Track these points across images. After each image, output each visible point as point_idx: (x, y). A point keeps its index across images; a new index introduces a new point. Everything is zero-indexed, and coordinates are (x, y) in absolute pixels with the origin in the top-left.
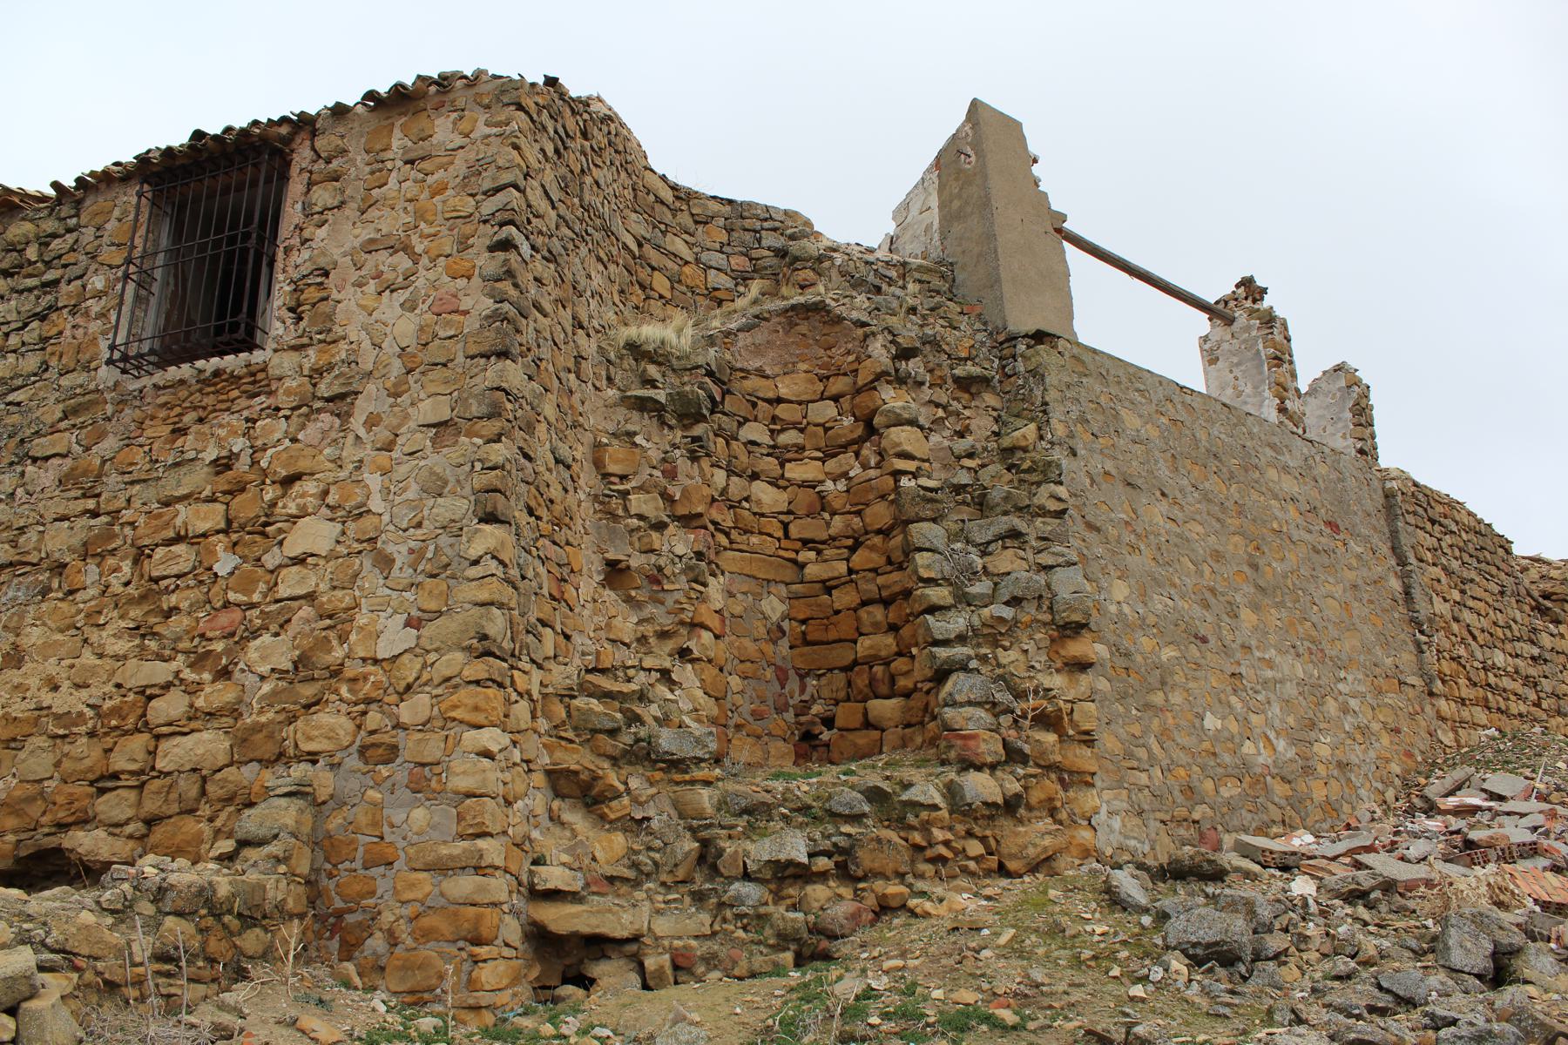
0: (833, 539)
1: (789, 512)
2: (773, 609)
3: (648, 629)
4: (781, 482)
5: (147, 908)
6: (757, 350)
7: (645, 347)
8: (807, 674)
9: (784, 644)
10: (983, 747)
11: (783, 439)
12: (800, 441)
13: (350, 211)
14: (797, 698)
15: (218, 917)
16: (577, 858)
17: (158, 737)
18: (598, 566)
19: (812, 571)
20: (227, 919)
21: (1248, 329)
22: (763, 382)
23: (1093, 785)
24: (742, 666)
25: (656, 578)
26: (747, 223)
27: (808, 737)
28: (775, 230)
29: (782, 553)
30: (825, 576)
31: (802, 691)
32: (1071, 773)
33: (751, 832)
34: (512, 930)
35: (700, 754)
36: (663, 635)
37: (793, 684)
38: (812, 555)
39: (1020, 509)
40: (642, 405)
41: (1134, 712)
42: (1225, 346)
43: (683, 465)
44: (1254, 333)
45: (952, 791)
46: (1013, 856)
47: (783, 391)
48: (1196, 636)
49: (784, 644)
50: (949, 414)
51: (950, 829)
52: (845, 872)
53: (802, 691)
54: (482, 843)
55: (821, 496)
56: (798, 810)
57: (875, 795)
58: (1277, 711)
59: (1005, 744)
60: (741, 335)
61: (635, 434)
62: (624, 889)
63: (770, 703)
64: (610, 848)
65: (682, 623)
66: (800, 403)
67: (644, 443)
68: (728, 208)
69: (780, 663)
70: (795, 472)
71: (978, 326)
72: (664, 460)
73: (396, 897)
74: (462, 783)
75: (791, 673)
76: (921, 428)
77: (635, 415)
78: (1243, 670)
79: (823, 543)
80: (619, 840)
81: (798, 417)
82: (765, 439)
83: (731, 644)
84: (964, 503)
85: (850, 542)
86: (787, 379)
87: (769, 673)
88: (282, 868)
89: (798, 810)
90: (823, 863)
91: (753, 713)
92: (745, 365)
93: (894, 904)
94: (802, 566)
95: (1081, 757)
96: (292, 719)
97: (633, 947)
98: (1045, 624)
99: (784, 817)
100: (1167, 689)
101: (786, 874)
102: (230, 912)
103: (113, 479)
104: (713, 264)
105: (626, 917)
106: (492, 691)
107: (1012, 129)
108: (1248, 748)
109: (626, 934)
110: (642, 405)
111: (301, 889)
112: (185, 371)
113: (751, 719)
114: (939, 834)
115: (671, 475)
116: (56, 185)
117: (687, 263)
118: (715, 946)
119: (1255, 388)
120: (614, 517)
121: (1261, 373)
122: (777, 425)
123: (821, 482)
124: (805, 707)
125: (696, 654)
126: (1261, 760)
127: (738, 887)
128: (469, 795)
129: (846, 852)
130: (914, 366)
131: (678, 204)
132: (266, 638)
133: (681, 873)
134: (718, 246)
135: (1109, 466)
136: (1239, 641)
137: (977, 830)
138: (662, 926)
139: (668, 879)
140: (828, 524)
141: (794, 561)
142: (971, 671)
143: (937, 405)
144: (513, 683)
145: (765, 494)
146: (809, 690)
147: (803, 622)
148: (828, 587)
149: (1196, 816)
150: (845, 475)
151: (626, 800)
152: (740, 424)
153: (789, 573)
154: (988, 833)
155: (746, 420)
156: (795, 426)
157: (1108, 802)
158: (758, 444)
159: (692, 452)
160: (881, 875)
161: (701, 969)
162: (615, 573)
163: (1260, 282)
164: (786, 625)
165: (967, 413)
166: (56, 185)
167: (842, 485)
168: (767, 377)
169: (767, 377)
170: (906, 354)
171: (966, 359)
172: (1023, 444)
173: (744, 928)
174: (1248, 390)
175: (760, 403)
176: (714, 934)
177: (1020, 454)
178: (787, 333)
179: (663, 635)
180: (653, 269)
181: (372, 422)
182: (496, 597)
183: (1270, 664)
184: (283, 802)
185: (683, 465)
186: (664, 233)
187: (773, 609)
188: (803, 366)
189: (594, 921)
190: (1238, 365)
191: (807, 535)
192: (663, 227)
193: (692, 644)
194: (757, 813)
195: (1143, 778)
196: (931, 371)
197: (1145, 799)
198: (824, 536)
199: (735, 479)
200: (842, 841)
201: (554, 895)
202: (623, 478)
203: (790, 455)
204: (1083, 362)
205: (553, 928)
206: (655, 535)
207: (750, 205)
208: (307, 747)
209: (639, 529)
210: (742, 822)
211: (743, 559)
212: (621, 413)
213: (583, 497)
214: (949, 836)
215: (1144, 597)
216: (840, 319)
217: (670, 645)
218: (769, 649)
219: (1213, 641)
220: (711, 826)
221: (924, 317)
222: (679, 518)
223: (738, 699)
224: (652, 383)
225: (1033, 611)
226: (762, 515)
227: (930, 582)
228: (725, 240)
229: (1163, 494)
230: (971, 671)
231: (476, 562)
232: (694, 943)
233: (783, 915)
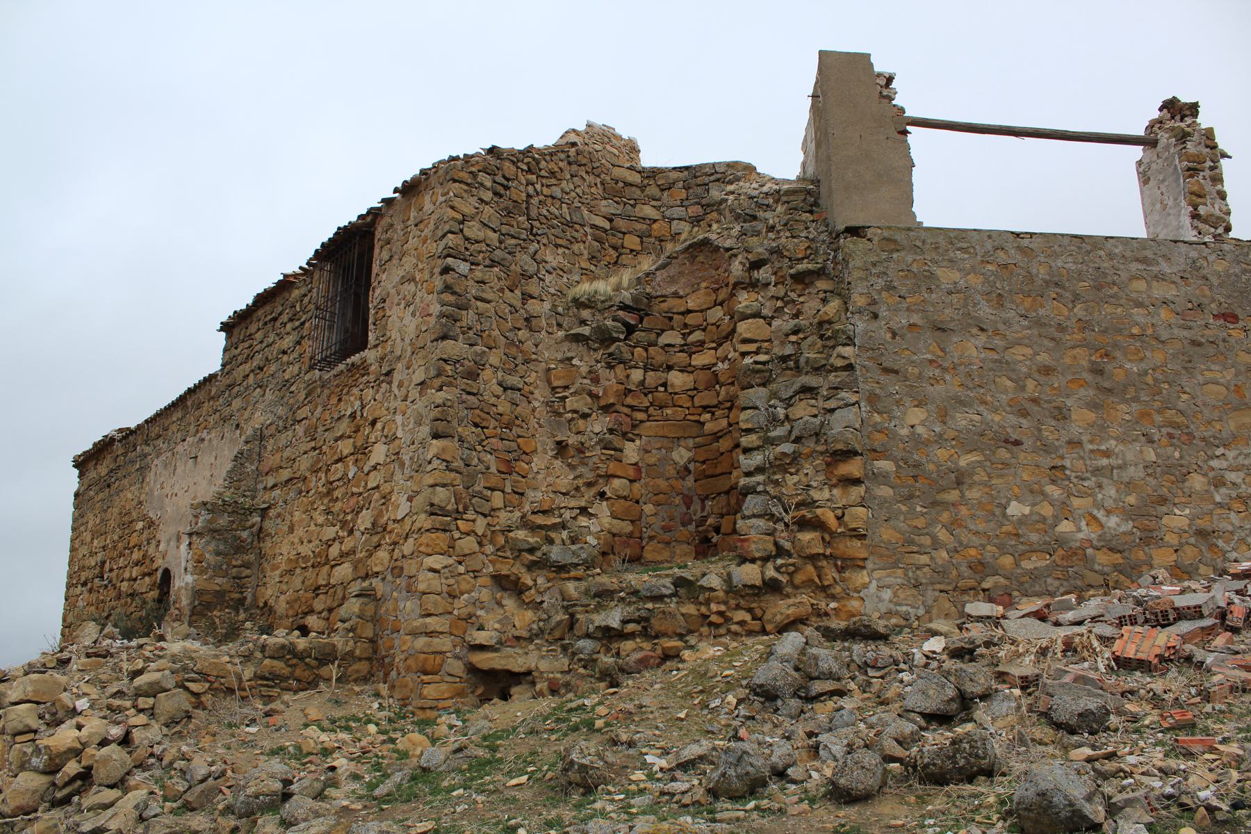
0: (720, 403)
1: (695, 389)
2: (681, 457)
3: (580, 482)
4: (689, 369)
5: (259, 655)
6: (672, 280)
7: (582, 300)
8: (707, 497)
9: (691, 478)
10: (753, 547)
11: (692, 338)
12: (702, 338)
13: (395, 261)
14: (699, 514)
15: (302, 659)
16: (503, 625)
17: (333, 567)
18: (551, 444)
19: (709, 427)
20: (307, 660)
21: (1167, 148)
22: (678, 301)
23: (864, 568)
24: (655, 498)
25: (581, 449)
26: (699, 181)
27: (706, 540)
28: (718, 180)
29: (689, 417)
30: (716, 430)
31: (703, 510)
32: (844, 560)
33: (599, 608)
34: (457, 667)
35: (575, 561)
36: (589, 485)
37: (696, 506)
38: (708, 416)
39: (817, 369)
40: (577, 338)
41: (919, 509)
42: (1154, 166)
43: (603, 373)
44: (1172, 150)
45: (728, 579)
46: (770, 621)
47: (691, 305)
48: (1006, 441)
49: (691, 478)
50: (786, 304)
51: (725, 603)
52: (645, 634)
53: (703, 510)
54: (428, 620)
55: (715, 375)
56: (632, 593)
57: (680, 582)
58: (1113, 492)
59: (776, 544)
60: (658, 273)
61: (572, 358)
62: (524, 644)
63: (678, 520)
64: (524, 619)
65: (601, 476)
66: (701, 311)
67: (578, 363)
68: (686, 173)
69: (686, 492)
70: (698, 360)
71: (823, 228)
72: (590, 372)
73: (404, 646)
74: (422, 587)
75: (695, 498)
76: (764, 318)
77: (574, 345)
78: (1067, 463)
79: (715, 407)
80: (530, 615)
81: (700, 320)
82: (679, 341)
83: (646, 485)
84: (787, 369)
85: (728, 404)
86: (694, 296)
87: (678, 500)
88: (351, 635)
89: (632, 593)
90: (631, 627)
91: (663, 528)
92: (664, 292)
93: (672, 653)
94: (703, 424)
95: (854, 548)
96: (371, 555)
97: (530, 678)
98: (822, 453)
99: (623, 599)
100: (965, 487)
101: (608, 635)
102: (310, 656)
103: (320, 429)
104: (675, 216)
105: (520, 660)
106: (441, 535)
107: (861, 61)
108: (1065, 527)
109: (522, 670)
110: (577, 338)
111: (366, 645)
112: (341, 367)
113: (661, 532)
114: (714, 607)
115: (596, 381)
116: (301, 268)
117: (655, 221)
118: (568, 677)
119: (1175, 200)
120: (559, 415)
121: (1178, 185)
122: (687, 330)
123: (715, 365)
124: (704, 519)
125: (609, 494)
126: (1081, 536)
127: (581, 643)
128: (424, 593)
129: (647, 620)
130: (763, 274)
131: (646, 182)
132: (364, 511)
133: (557, 634)
134: (679, 203)
135: (915, 319)
136: (1064, 439)
137: (742, 602)
138: (544, 665)
139: (550, 638)
140: (718, 394)
141: (698, 422)
142: (759, 493)
143: (778, 299)
144: (458, 528)
145: (677, 379)
146: (707, 508)
147: (704, 462)
148: (717, 436)
149: (985, 585)
150: (726, 358)
151: (533, 591)
152: (658, 335)
153: (695, 430)
154: (753, 605)
155: (663, 331)
156: (698, 327)
157: (878, 580)
158: (673, 346)
159: (608, 363)
160: (665, 635)
161: (563, 691)
162: (561, 448)
163: (1185, 98)
164: (691, 466)
165: (801, 299)
166: (301, 268)
167: (726, 366)
168: (681, 297)
169: (681, 297)
170: (757, 265)
171: (803, 259)
172: (826, 318)
173: (585, 667)
174: (1171, 203)
175: (675, 316)
176: (570, 670)
177: (826, 326)
178: (692, 263)
179: (589, 485)
180: (624, 234)
181: (400, 386)
182: (439, 481)
183: (1107, 454)
184: (354, 600)
185: (603, 373)
186: (633, 206)
187: (681, 457)
188: (704, 285)
189: (503, 662)
190: (1163, 181)
191: (705, 403)
192: (632, 202)
193: (606, 489)
194: (604, 596)
195: (924, 559)
196: (775, 274)
197: (924, 575)
198: (715, 402)
199: (651, 373)
200: (643, 613)
201: (482, 648)
202: (566, 387)
203: (694, 349)
204: (895, 241)
205: (479, 666)
206: (581, 422)
207: (701, 166)
208: (375, 569)
209: (573, 419)
210: (593, 603)
211: (657, 426)
212: (566, 345)
213: (536, 404)
214: (723, 608)
215: (943, 416)
216: (718, 248)
217: (593, 491)
218: (678, 484)
219: (1028, 443)
220: (575, 605)
221: (778, 232)
222: (602, 408)
223: (652, 520)
224: (583, 322)
225: (812, 445)
226: (676, 393)
227: (748, 431)
228: (684, 196)
229: (982, 330)
230: (759, 493)
231: (430, 463)
232: (559, 675)
233: (607, 660)
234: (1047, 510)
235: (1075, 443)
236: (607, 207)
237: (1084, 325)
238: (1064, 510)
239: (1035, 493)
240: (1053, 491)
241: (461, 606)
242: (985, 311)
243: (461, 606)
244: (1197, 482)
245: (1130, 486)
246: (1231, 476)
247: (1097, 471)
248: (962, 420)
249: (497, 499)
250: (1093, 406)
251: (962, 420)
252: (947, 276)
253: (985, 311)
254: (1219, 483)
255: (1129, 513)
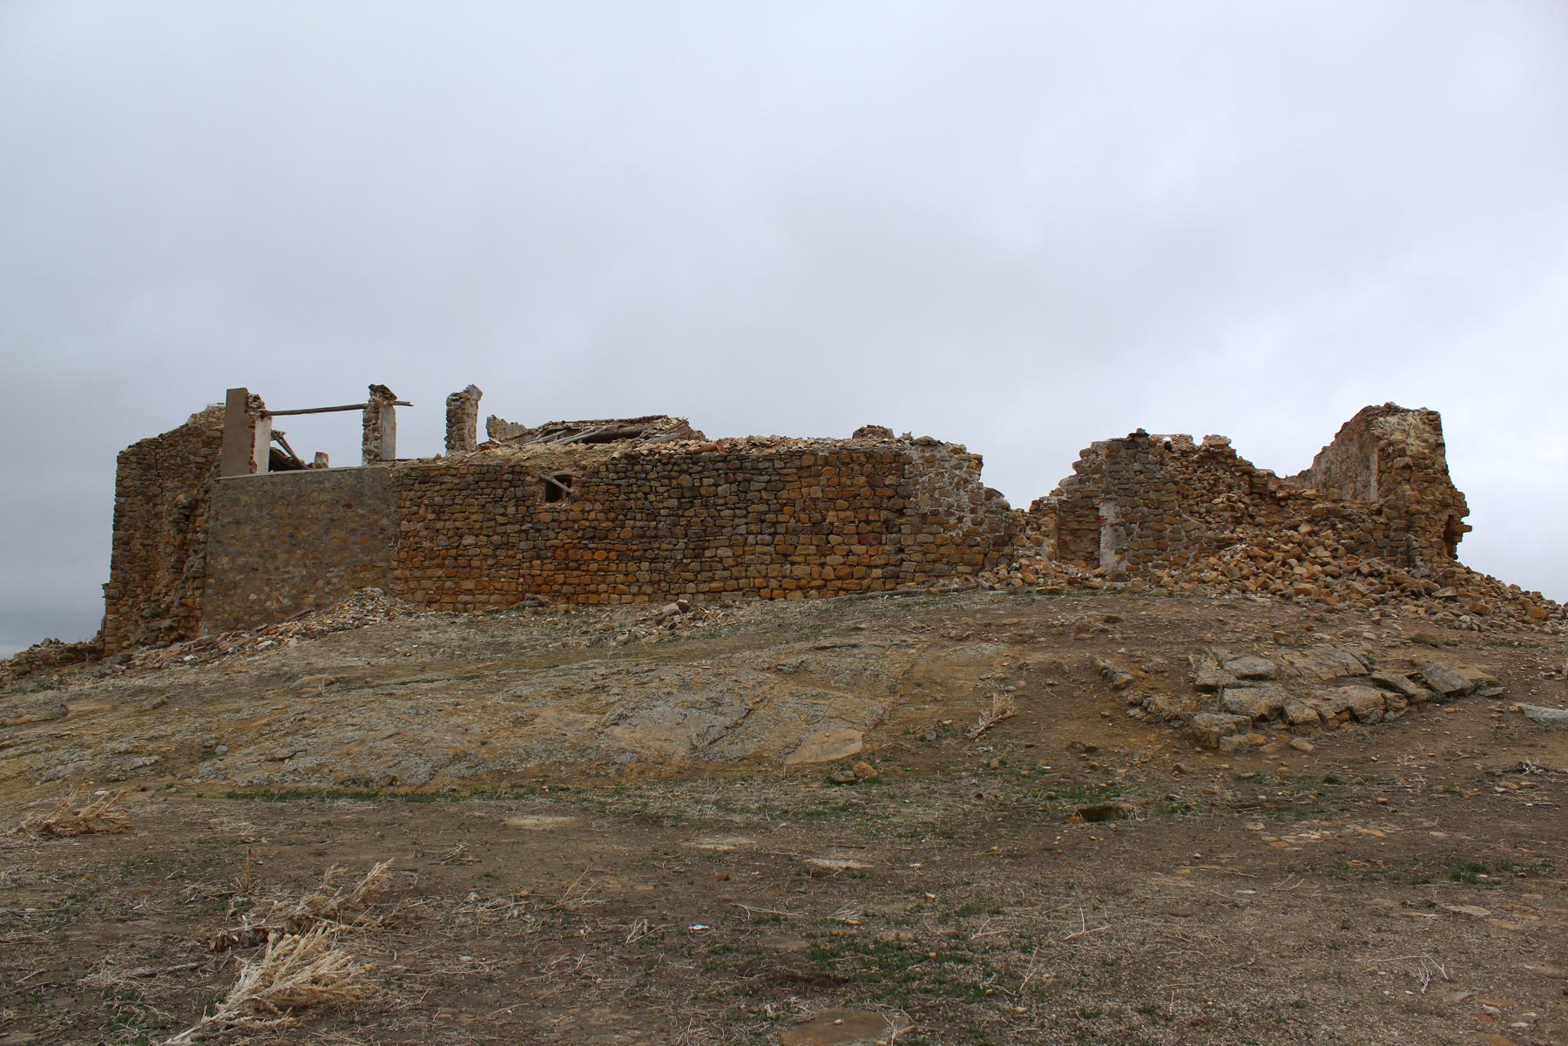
95: (198, 613)
234: (263, 597)
235: (277, 569)
236: (205, 451)
237: (290, 516)
238: (269, 597)
239: (259, 590)
240: (266, 589)
241: (121, 632)
242: (255, 513)
243: (121, 632)
244: (321, 583)
245: (294, 586)
246: (335, 580)
247: (283, 580)
248: (241, 561)
249: (139, 591)
250: (289, 552)
251: (241, 561)
252: (244, 498)
253: (255, 513)
254: (328, 583)
255: (293, 598)
